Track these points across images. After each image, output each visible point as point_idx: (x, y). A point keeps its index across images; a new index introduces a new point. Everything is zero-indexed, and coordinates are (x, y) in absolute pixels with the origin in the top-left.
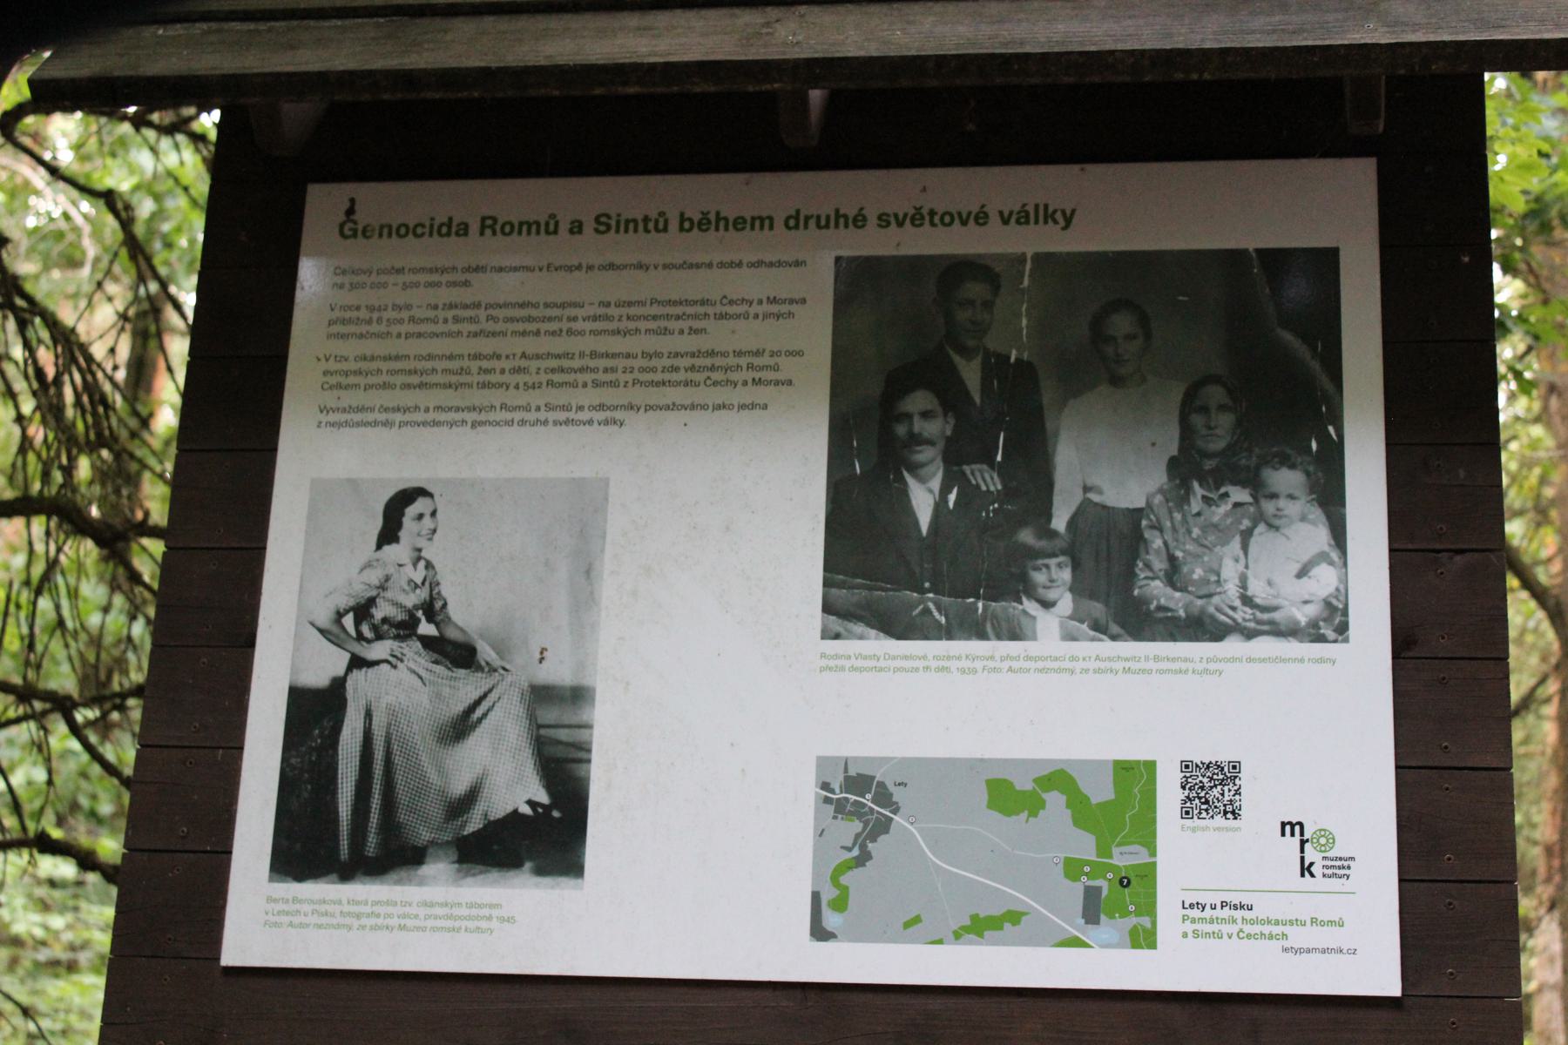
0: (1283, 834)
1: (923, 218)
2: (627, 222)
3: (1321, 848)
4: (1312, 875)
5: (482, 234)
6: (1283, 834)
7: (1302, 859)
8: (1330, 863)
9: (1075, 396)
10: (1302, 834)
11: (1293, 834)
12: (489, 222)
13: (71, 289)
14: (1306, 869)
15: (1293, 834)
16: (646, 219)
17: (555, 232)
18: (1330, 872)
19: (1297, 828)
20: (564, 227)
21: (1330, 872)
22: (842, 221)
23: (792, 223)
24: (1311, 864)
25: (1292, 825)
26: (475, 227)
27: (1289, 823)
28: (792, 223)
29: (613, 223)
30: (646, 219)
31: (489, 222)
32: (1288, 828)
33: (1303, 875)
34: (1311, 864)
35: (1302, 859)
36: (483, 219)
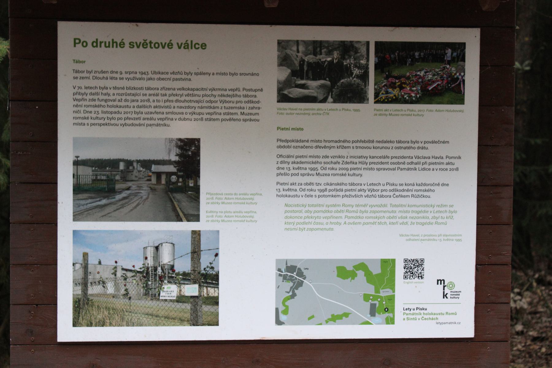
0: (438, 284)
1: (147, 44)
6: (438, 284)
7: (444, 292)
10: (444, 284)
11: (441, 284)
14: (445, 296)
15: (441, 284)
18: (453, 296)
19: (442, 282)
21: (453, 296)
22: (115, 44)
23: (95, 44)
25: (441, 281)
28: (95, 44)
32: (439, 282)
35: (444, 292)
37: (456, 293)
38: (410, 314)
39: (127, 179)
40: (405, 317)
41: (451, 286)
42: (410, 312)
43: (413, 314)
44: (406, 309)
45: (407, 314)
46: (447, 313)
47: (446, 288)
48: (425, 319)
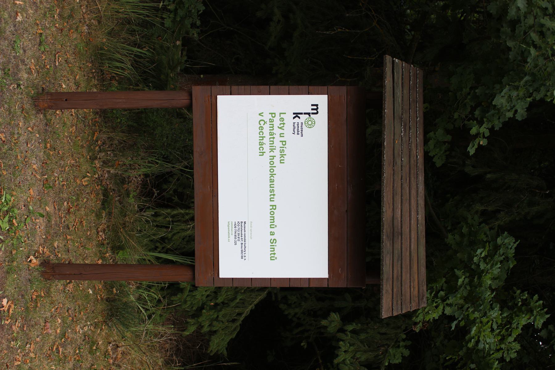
0: (312, 105)
2: (274, 248)
3: (306, 122)
4: (294, 118)
5: (271, 206)
6: (312, 105)
7: (301, 114)
8: (300, 126)
9: (383, 66)
10: (313, 113)
11: (312, 109)
12: (274, 207)
13: (58, 190)
14: (297, 115)
15: (312, 109)
16: (274, 254)
17: (271, 227)
18: (296, 126)
19: (315, 111)
20: (272, 230)
21: (296, 126)
24: (299, 118)
25: (317, 109)
26: (272, 203)
27: (317, 108)
29: (274, 244)
30: (274, 254)
31: (274, 207)
32: (315, 107)
33: (294, 114)
34: (299, 118)
35: (301, 114)
36: (275, 206)
37: (300, 129)
38: (272, 127)
39: (91, 289)
40: (267, 117)
41: (310, 123)
42: (275, 127)
43: (271, 134)
44: (282, 119)
45: (271, 121)
46: (274, 207)
47: (307, 116)
48: (261, 128)
